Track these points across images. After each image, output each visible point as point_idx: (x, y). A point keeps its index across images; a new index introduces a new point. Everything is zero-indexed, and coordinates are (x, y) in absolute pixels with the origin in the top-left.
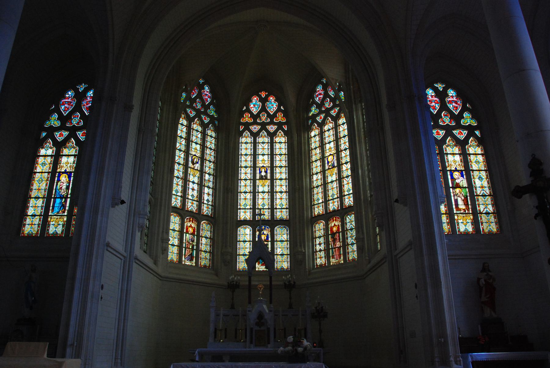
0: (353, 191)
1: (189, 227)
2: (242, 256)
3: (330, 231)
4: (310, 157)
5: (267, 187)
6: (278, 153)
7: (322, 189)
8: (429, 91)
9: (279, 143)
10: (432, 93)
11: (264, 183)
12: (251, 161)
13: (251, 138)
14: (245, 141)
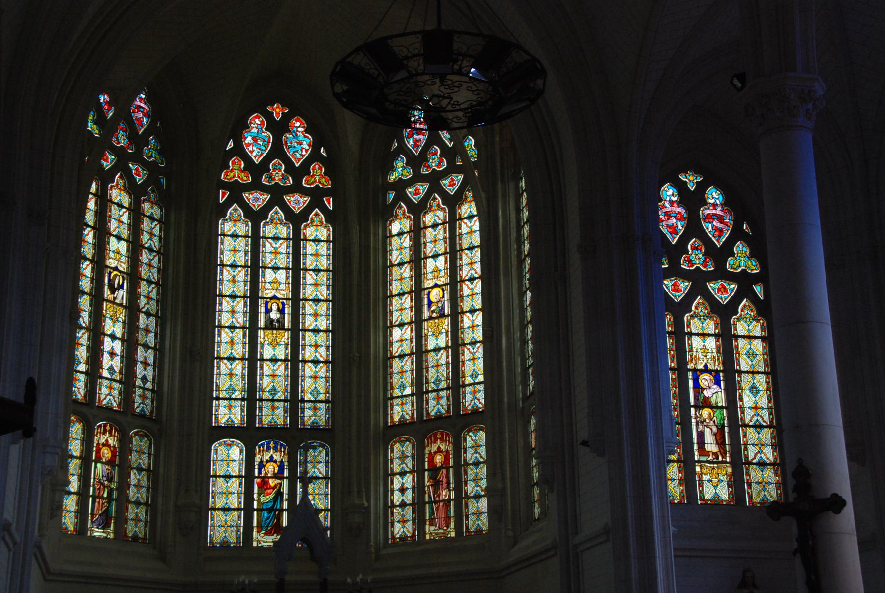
0: (484, 377)
1: (104, 445)
2: (221, 513)
3: (428, 461)
4: (386, 283)
5: (283, 348)
6: (311, 265)
7: (412, 363)
8: (666, 191)
9: (314, 240)
10: (673, 195)
11: (275, 338)
12: (245, 282)
13: (247, 225)
14: (232, 230)
